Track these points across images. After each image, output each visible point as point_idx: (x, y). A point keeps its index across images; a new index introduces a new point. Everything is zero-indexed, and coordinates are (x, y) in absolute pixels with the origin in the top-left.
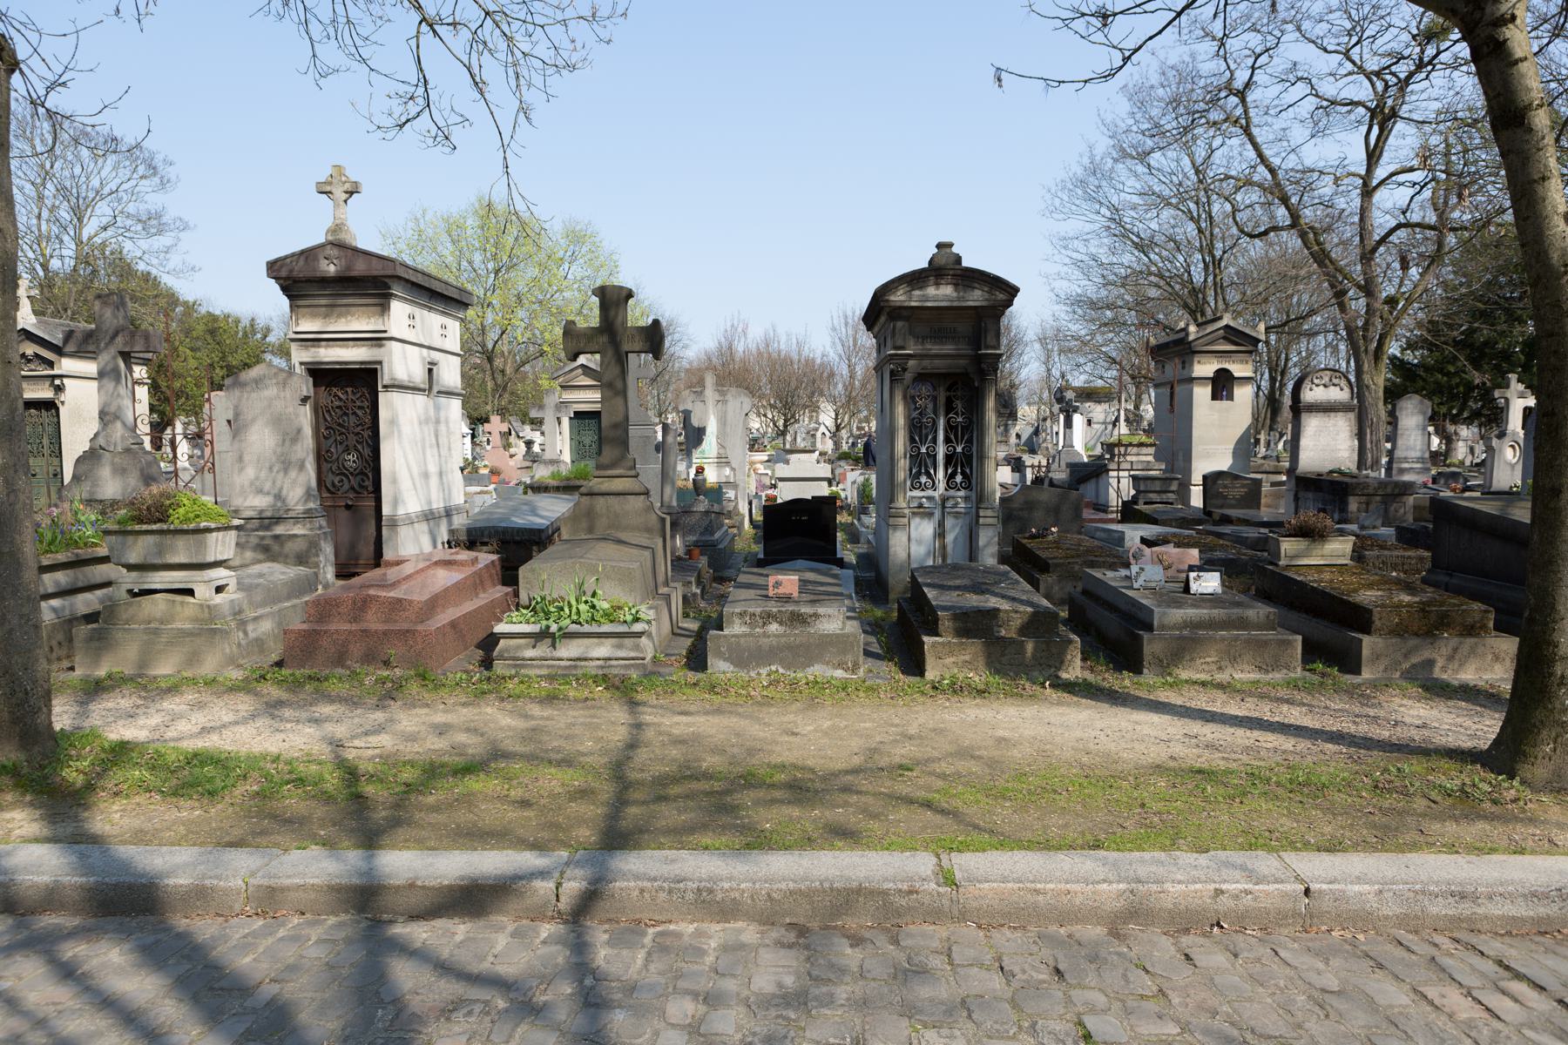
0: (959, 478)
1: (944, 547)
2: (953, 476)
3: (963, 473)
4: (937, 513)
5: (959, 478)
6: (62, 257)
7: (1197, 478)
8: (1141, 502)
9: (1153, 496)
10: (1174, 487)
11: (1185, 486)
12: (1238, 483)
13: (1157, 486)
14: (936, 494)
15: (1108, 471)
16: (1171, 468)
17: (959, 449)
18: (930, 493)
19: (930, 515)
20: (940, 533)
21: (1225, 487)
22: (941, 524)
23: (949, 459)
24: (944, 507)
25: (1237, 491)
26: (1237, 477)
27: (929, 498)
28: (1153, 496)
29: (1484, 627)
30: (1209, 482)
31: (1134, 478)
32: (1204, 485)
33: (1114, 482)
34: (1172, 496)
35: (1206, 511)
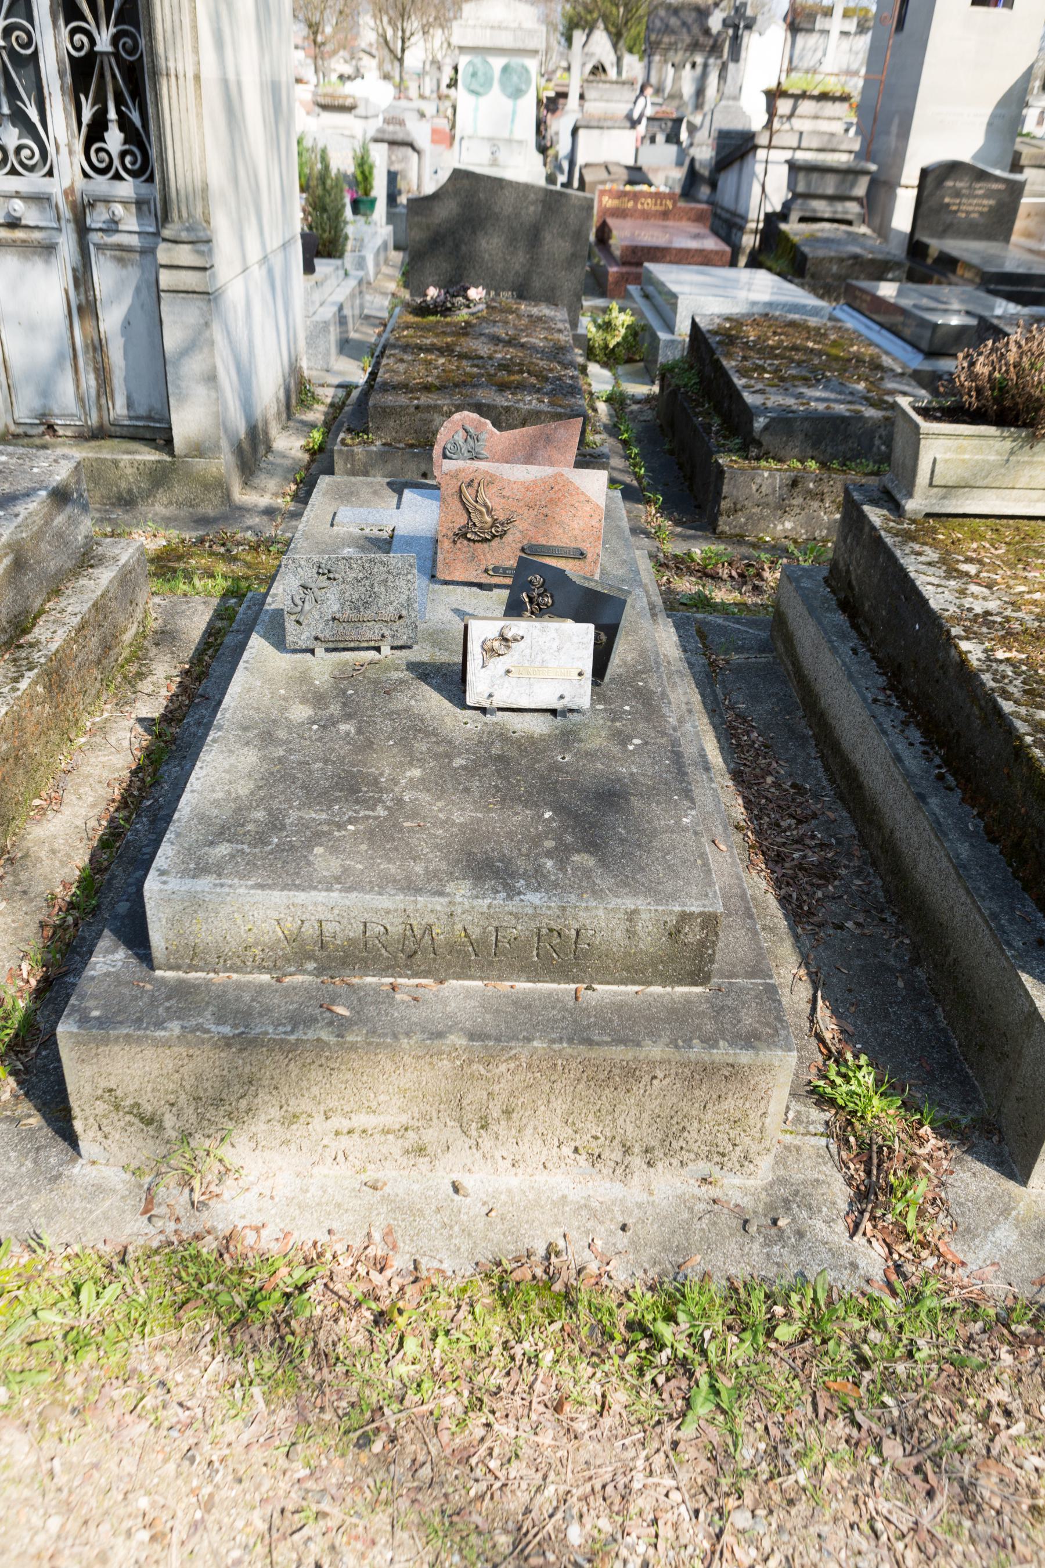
0: (114, 139)
1: (98, 347)
2: (96, 132)
3: (124, 123)
4: (67, 243)
5: (114, 139)
6: (197, 1329)
7: (910, 176)
8: (794, 216)
9: (821, 207)
10: (861, 189)
11: (882, 188)
12: (981, 188)
13: (830, 184)
14: (55, 187)
15: (755, 147)
16: (866, 153)
17: (104, 43)
18: (31, 182)
19: (48, 249)
20: (84, 306)
21: (957, 194)
22: (82, 277)
23: (82, 71)
24: (83, 231)
25: (974, 204)
26: (982, 176)
27: (40, 199)
28: (821, 207)
29: (565, 398)
30: (930, 180)
31: (794, 167)
32: (921, 187)
33: (759, 168)
34: (853, 209)
35: (916, 248)
